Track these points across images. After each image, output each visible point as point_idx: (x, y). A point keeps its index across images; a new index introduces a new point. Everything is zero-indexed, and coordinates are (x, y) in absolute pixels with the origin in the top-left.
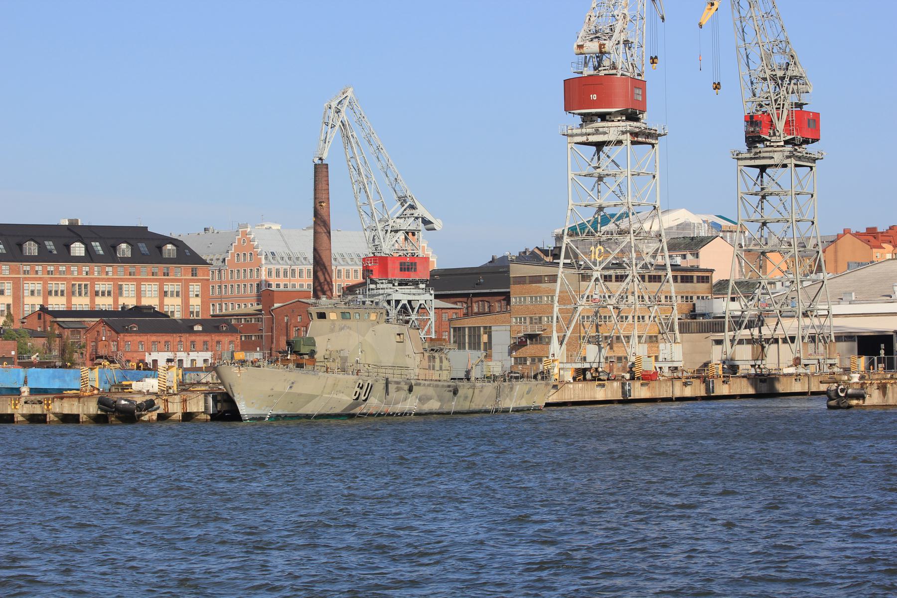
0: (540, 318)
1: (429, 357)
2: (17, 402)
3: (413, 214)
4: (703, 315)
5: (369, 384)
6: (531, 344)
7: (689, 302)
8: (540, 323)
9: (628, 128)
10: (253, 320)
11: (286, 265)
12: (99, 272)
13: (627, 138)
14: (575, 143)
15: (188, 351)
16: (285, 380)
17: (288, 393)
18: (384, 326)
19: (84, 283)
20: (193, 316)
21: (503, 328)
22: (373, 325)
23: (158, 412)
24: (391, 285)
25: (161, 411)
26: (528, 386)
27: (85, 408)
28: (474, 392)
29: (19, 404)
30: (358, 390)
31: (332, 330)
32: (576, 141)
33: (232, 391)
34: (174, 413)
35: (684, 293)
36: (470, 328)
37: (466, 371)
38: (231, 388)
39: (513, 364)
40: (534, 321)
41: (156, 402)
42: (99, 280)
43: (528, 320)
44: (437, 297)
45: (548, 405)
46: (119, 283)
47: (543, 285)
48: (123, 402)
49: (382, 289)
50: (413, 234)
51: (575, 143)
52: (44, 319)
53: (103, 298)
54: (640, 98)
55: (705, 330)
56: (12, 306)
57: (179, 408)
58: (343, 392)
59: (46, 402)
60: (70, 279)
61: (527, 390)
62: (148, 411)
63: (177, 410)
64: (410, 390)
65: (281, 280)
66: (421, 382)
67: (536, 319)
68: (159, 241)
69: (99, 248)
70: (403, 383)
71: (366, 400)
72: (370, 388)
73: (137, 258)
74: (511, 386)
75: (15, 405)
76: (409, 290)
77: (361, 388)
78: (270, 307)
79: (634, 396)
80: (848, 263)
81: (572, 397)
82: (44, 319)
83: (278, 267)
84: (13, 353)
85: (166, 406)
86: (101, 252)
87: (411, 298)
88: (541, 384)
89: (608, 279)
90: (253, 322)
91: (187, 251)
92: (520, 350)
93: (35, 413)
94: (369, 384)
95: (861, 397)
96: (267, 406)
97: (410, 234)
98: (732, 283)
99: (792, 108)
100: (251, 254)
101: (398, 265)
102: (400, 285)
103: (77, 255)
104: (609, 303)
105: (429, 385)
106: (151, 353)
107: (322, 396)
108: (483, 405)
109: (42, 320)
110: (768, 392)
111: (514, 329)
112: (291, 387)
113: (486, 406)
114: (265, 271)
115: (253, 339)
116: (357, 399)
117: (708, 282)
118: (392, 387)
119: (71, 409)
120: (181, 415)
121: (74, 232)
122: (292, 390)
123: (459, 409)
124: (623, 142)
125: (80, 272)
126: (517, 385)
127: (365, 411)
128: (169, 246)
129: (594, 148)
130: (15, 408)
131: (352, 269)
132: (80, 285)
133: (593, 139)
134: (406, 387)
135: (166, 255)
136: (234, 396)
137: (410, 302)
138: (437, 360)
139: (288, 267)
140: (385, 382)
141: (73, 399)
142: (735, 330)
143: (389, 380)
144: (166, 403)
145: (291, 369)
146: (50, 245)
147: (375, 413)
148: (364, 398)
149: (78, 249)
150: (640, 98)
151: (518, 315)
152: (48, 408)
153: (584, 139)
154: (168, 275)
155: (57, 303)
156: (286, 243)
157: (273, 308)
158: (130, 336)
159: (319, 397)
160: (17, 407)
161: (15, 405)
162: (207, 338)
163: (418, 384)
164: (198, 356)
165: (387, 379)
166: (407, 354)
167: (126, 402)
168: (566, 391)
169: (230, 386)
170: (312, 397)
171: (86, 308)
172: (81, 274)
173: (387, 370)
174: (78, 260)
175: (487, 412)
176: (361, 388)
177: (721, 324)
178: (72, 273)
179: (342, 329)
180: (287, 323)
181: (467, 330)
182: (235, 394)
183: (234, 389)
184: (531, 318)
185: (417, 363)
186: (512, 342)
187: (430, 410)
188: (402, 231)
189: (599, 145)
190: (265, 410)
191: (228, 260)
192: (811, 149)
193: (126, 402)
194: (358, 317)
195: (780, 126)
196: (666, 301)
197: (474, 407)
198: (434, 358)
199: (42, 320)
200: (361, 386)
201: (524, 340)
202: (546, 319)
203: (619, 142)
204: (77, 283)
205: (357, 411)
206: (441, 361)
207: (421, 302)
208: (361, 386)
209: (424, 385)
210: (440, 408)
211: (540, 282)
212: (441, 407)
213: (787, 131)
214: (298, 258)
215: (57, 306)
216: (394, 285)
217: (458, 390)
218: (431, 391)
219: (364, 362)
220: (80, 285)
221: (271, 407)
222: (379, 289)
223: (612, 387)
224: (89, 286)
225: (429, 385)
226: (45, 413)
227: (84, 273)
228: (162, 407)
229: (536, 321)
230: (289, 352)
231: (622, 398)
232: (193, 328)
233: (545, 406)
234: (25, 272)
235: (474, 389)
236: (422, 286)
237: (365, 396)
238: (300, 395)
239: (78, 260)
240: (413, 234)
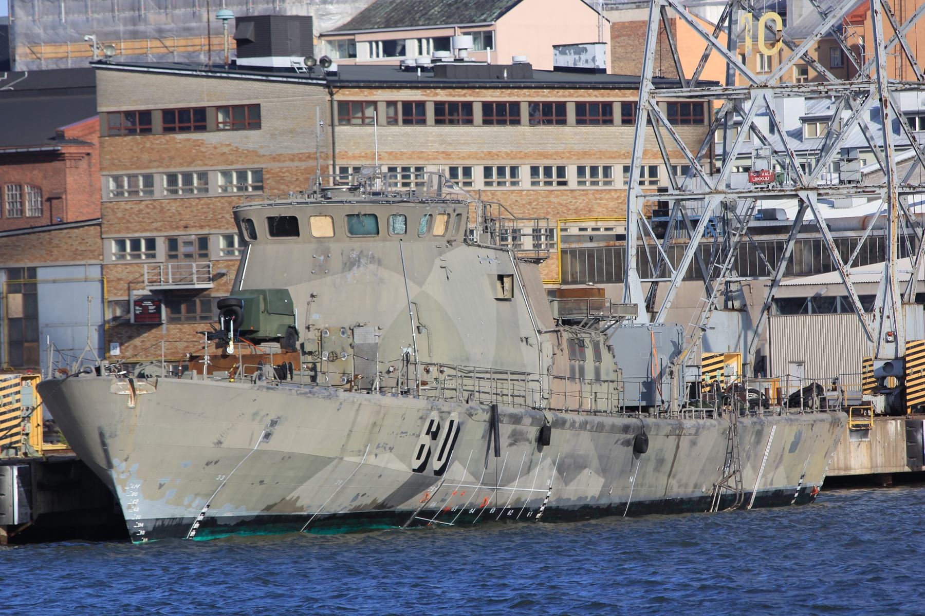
0: (203, 242)
1: (571, 341)
5: (452, 422)
6: (171, 320)
8: (205, 256)
16: (256, 414)
17: (259, 454)
18: (461, 254)
21: (79, 272)
22: (440, 251)
26: (795, 429)
28: (678, 447)
30: (426, 440)
31: (321, 270)
33: (106, 452)
37: (645, 384)
38: (104, 444)
40: (182, 249)
43: (161, 247)
45: (832, 483)
47: (209, 138)
58: (391, 449)
61: (792, 439)
64: (543, 439)
66: (569, 416)
67: (190, 243)
70: (527, 421)
71: (440, 472)
72: (456, 432)
74: (758, 427)
77: (435, 436)
80: (378, 233)
81: (880, 460)
86: (505, 71)
88: (822, 421)
89: (414, 117)
92: (137, 341)
94: (452, 422)
96: (197, 495)
104: (805, 183)
105: (583, 426)
107: (342, 459)
108: (695, 486)
111: (112, 274)
112: (267, 436)
113: (701, 487)
116: (422, 468)
117: (701, 122)
118: (505, 429)
122: (272, 445)
123: (646, 494)
126: (771, 424)
127: (433, 505)
134: (533, 432)
136: (110, 465)
138: (589, 352)
140: (487, 417)
143: (501, 409)
147: (454, 509)
148: (437, 465)
151: (128, 229)
159: (336, 461)
163: (560, 423)
165: (494, 408)
166: (523, 335)
169: (102, 435)
170: (317, 463)
173: (482, 383)
175: (700, 504)
176: (435, 436)
179: (350, 264)
182: (115, 461)
183: (114, 447)
184: (173, 243)
185: (547, 361)
186: (109, 316)
187: (580, 499)
190: (189, 506)
194: (399, 224)
196: (580, 183)
197: (677, 490)
198: (582, 345)
200: (434, 429)
201: (152, 308)
202: (222, 243)
205: (415, 503)
206: (598, 357)
208: (434, 429)
209: (573, 424)
210: (602, 494)
211: (202, 128)
212: (604, 492)
217: (646, 441)
218: (585, 444)
219: (428, 361)
221: (208, 495)
223: (885, 434)
225: (583, 426)
229: (190, 249)
230: (231, 334)
231: (907, 469)
233: (824, 488)
235: (679, 436)
237: (440, 459)
238: (287, 458)
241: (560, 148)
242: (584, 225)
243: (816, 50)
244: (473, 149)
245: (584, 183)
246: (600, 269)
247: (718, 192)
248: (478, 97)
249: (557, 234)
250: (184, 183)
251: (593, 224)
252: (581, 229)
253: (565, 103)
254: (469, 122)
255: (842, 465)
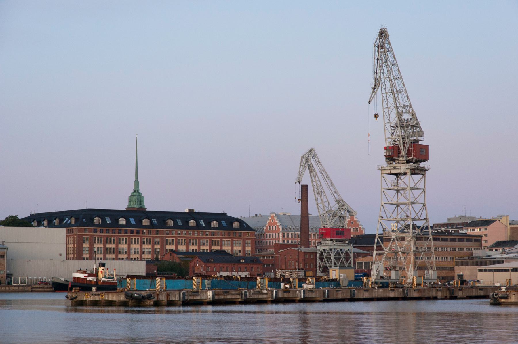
2: (88, 295)
3: (343, 208)
4: (476, 257)
7: (454, 251)
9: (409, 167)
10: (270, 257)
11: (292, 232)
12: (185, 234)
13: (408, 172)
14: (385, 174)
15: (237, 271)
19: (217, 240)
20: (247, 255)
23: (154, 300)
24: (331, 242)
25: (155, 299)
27: (119, 297)
29: (89, 296)
32: (385, 173)
34: (164, 300)
35: (451, 246)
36: (365, 262)
39: (258, 278)
41: (153, 295)
42: (202, 238)
44: (354, 247)
46: (212, 239)
48: (136, 295)
49: (328, 243)
50: (343, 218)
51: (385, 174)
52: (173, 255)
53: (216, 247)
54: (425, 154)
55: (475, 265)
56: (115, 249)
57: (165, 298)
59: (101, 295)
60: (188, 237)
62: (149, 300)
63: (164, 299)
65: (290, 239)
68: (231, 220)
69: (203, 223)
73: (220, 227)
75: (87, 296)
76: (340, 244)
78: (278, 251)
79: (410, 296)
81: (377, 296)
82: (173, 255)
83: (291, 233)
84: (155, 271)
85: (159, 297)
86: (204, 225)
87: (341, 248)
90: (270, 258)
91: (245, 225)
93: (96, 300)
95: (506, 298)
97: (342, 218)
98: (377, 237)
99: (411, 142)
100: (276, 226)
101: (335, 232)
102: (336, 241)
103: (122, 224)
106: (220, 272)
109: (172, 256)
110: (484, 295)
114: (282, 234)
115: (270, 266)
119: (113, 298)
120: (166, 301)
121: (191, 214)
124: (407, 173)
125: (193, 234)
128: (236, 222)
129: (395, 177)
130: (87, 297)
131: (312, 234)
132: (215, 241)
133: (393, 172)
135: (234, 226)
137: (341, 250)
139: (293, 233)
141: (114, 293)
142: (331, 249)
144: (158, 296)
145: (50, 278)
146: (202, 223)
149: (192, 223)
150: (425, 154)
152: (102, 297)
153: (388, 172)
154: (213, 236)
155: (182, 248)
156: (292, 222)
157: (279, 252)
158: (210, 264)
160: (88, 297)
161: (87, 296)
162: (246, 266)
164: (242, 274)
167: (137, 295)
168: (373, 293)
171: (185, 251)
172: (200, 235)
174: (192, 228)
177: (485, 262)
178: (189, 234)
180: (286, 259)
181: (364, 263)
188: (338, 216)
189: (397, 175)
191: (265, 229)
192: (422, 165)
193: (137, 295)
195: (403, 153)
196: (450, 251)
199: (172, 256)
203: (405, 174)
204: (214, 239)
207: (346, 250)
213: (408, 155)
214: (290, 229)
215: (182, 250)
216: (333, 242)
220: (215, 241)
222: (326, 243)
224: (220, 241)
226: (101, 300)
227: (184, 234)
228: (156, 297)
232: (240, 261)
234: (166, 234)
236: (347, 242)
239: (192, 228)
240: (343, 218)
241: (455, 245)
242: (459, 257)
243: (10, 216)
244: (440, 245)
245: (443, 250)
246: (474, 264)
247: (387, 252)
248: (441, 237)
249: (454, 259)
250: (427, 249)
251: (460, 257)
252: (458, 258)
253: (456, 238)
254: (439, 241)
255: (388, 295)
